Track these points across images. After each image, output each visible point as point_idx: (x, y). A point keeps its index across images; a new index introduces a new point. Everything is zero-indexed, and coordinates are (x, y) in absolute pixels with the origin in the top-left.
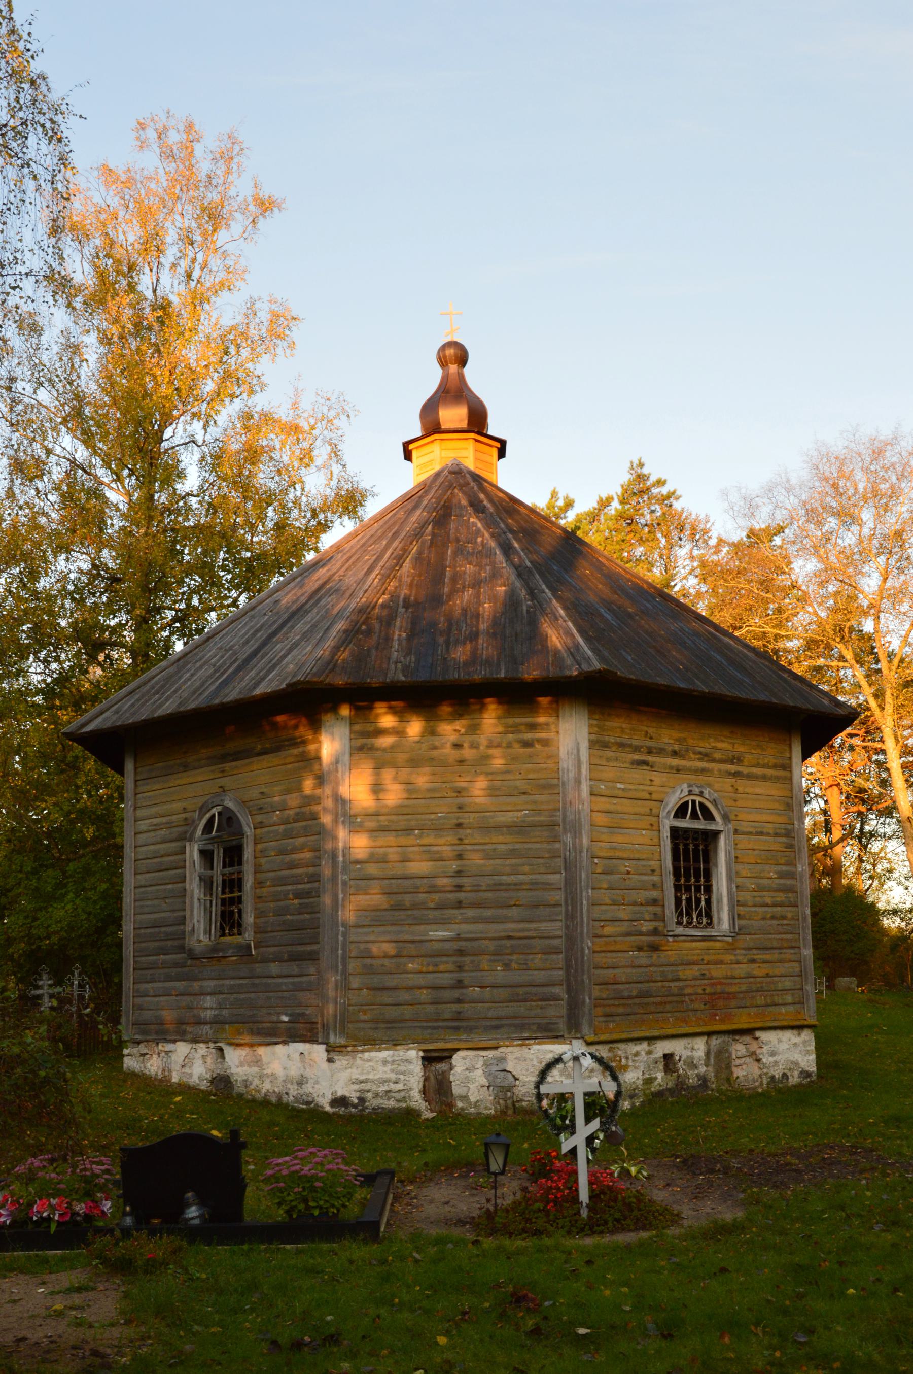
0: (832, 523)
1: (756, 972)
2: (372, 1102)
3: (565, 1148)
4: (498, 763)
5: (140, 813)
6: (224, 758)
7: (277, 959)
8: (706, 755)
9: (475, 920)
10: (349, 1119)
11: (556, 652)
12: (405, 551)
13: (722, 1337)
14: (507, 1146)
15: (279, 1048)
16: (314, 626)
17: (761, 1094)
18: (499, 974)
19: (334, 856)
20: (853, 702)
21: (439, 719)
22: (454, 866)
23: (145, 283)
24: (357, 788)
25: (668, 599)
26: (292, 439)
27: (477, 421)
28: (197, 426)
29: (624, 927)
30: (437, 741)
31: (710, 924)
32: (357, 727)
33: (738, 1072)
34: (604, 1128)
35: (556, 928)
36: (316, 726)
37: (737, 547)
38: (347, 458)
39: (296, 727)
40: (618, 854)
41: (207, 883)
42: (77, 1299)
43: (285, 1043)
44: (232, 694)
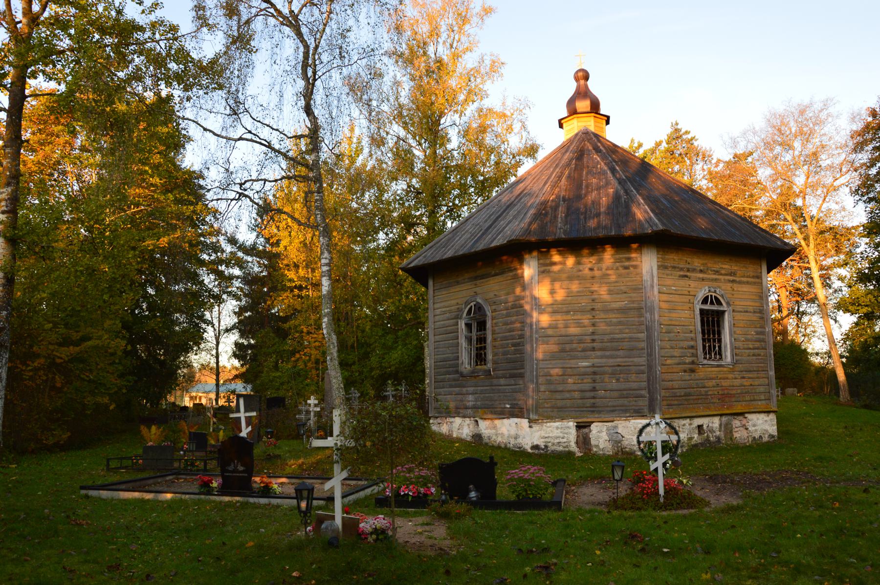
0: (778, 149)
1: (745, 383)
2: (551, 448)
3: (652, 468)
4: (613, 278)
5: (437, 306)
6: (476, 278)
7: (504, 377)
8: (717, 272)
9: (602, 357)
10: (540, 455)
11: (640, 221)
12: (562, 173)
13: (735, 553)
14: (623, 467)
15: (505, 421)
16: (519, 212)
17: (749, 446)
18: (614, 384)
19: (531, 325)
20: (792, 242)
21: (583, 256)
22: (591, 329)
23: (431, 50)
24: (542, 292)
25: (694, 192)
26: (502, 120)
27: (595, 107)
28: (457, 116)
29: (676, 360)
30: (581, 267)
31: (721, 358)
32: (541, 261)
33: (736, 435)
34: (671, 458)
35: (642, 360)
36: (521, 261)
37: (728, 163)
38: (529, 129)
39: (512, 262)
40: (673, 323)
41: (469, 340)
42: (427, 528)
43: (508, 418)
44: (481, 246)
